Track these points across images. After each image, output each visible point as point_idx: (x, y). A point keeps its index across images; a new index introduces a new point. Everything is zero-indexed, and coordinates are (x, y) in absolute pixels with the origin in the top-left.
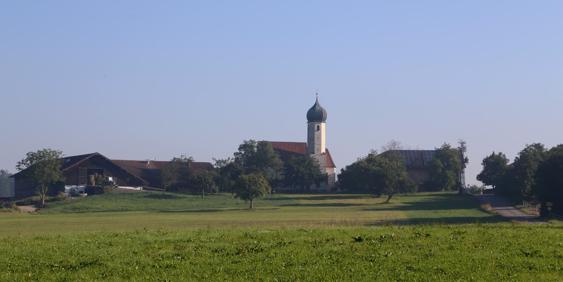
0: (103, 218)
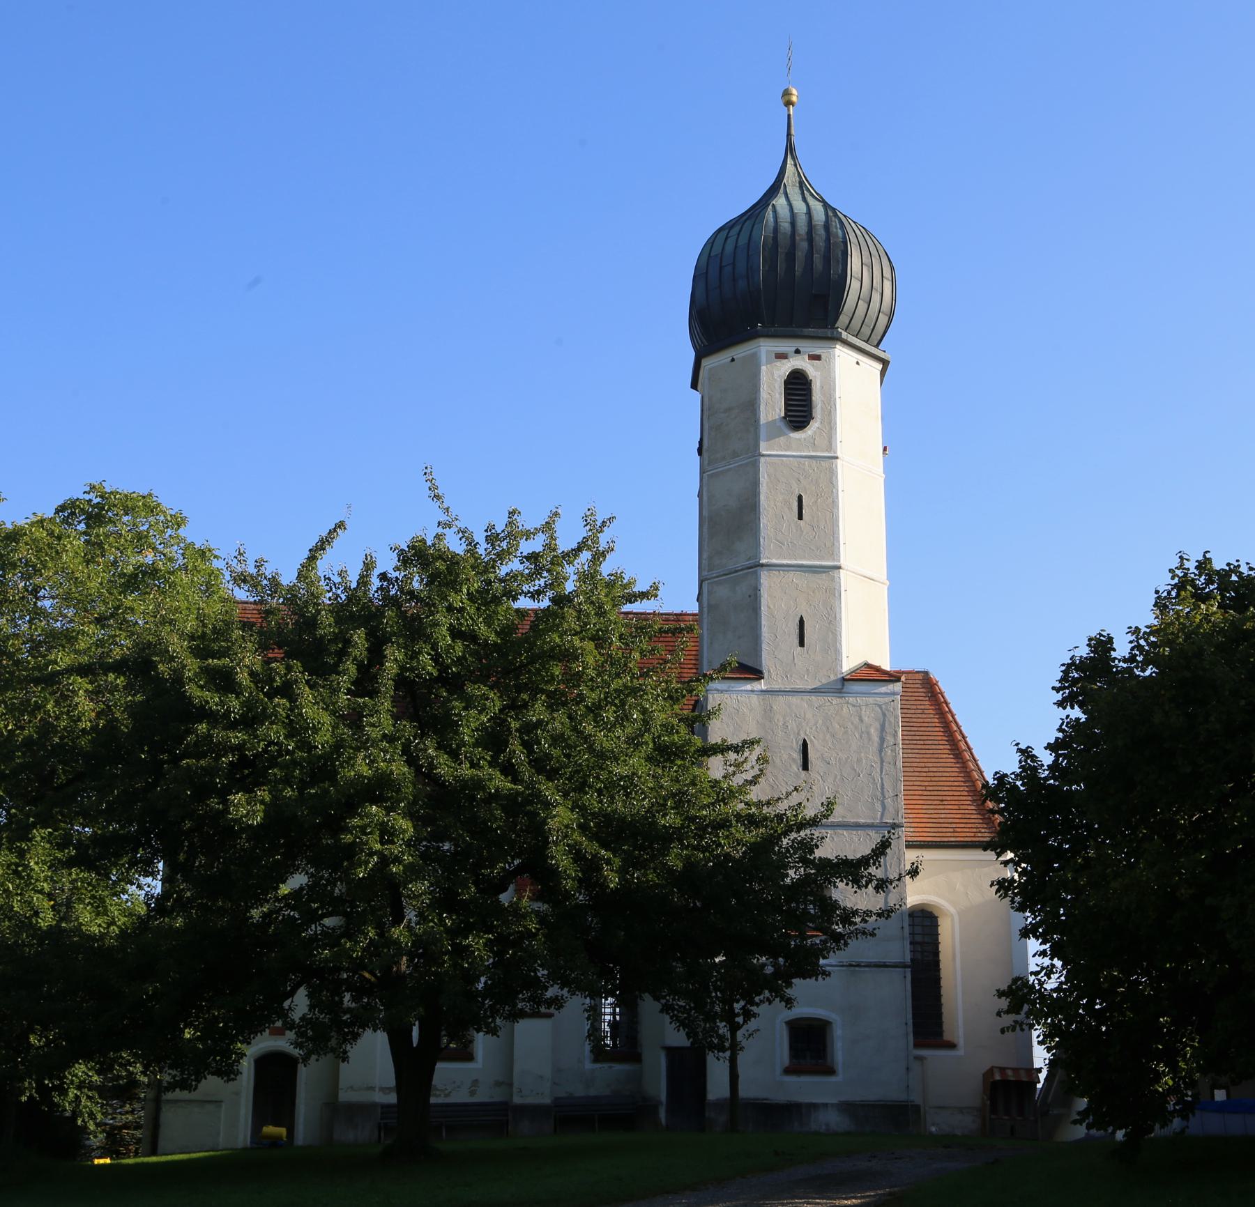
0: (878, 699)
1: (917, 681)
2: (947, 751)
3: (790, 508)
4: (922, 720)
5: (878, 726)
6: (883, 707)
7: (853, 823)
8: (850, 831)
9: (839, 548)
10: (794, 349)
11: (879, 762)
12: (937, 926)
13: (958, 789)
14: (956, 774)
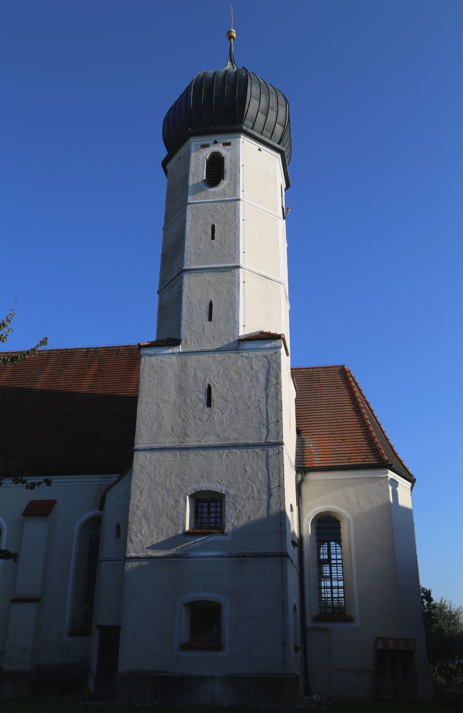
1: (336, 371)
2: (351, 409)
3: (206, 234)
4: (336, 393)
5: (264, 371)
6: (269, 357)
7: (244, 443)
8: (241, 450)
9: (239, 255)
10: (213, 141)
11: (265, 397)
12: (340, 528)
13: (356, 431)
14: (356, 423)
